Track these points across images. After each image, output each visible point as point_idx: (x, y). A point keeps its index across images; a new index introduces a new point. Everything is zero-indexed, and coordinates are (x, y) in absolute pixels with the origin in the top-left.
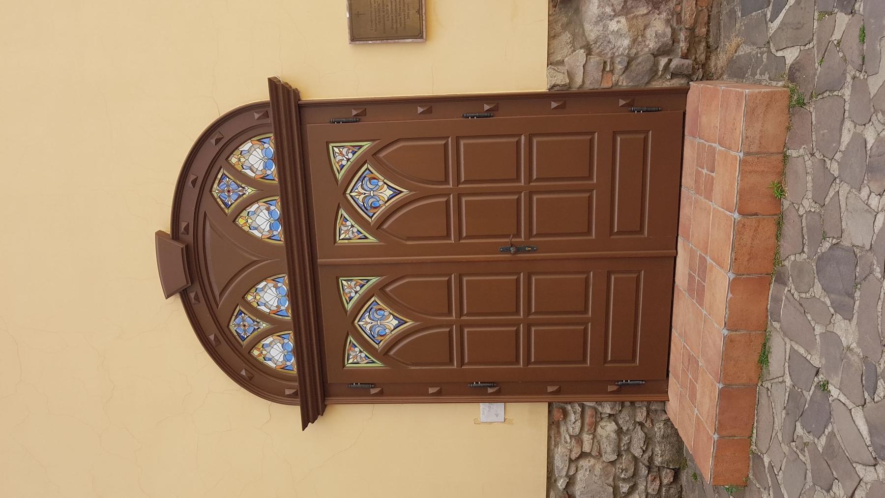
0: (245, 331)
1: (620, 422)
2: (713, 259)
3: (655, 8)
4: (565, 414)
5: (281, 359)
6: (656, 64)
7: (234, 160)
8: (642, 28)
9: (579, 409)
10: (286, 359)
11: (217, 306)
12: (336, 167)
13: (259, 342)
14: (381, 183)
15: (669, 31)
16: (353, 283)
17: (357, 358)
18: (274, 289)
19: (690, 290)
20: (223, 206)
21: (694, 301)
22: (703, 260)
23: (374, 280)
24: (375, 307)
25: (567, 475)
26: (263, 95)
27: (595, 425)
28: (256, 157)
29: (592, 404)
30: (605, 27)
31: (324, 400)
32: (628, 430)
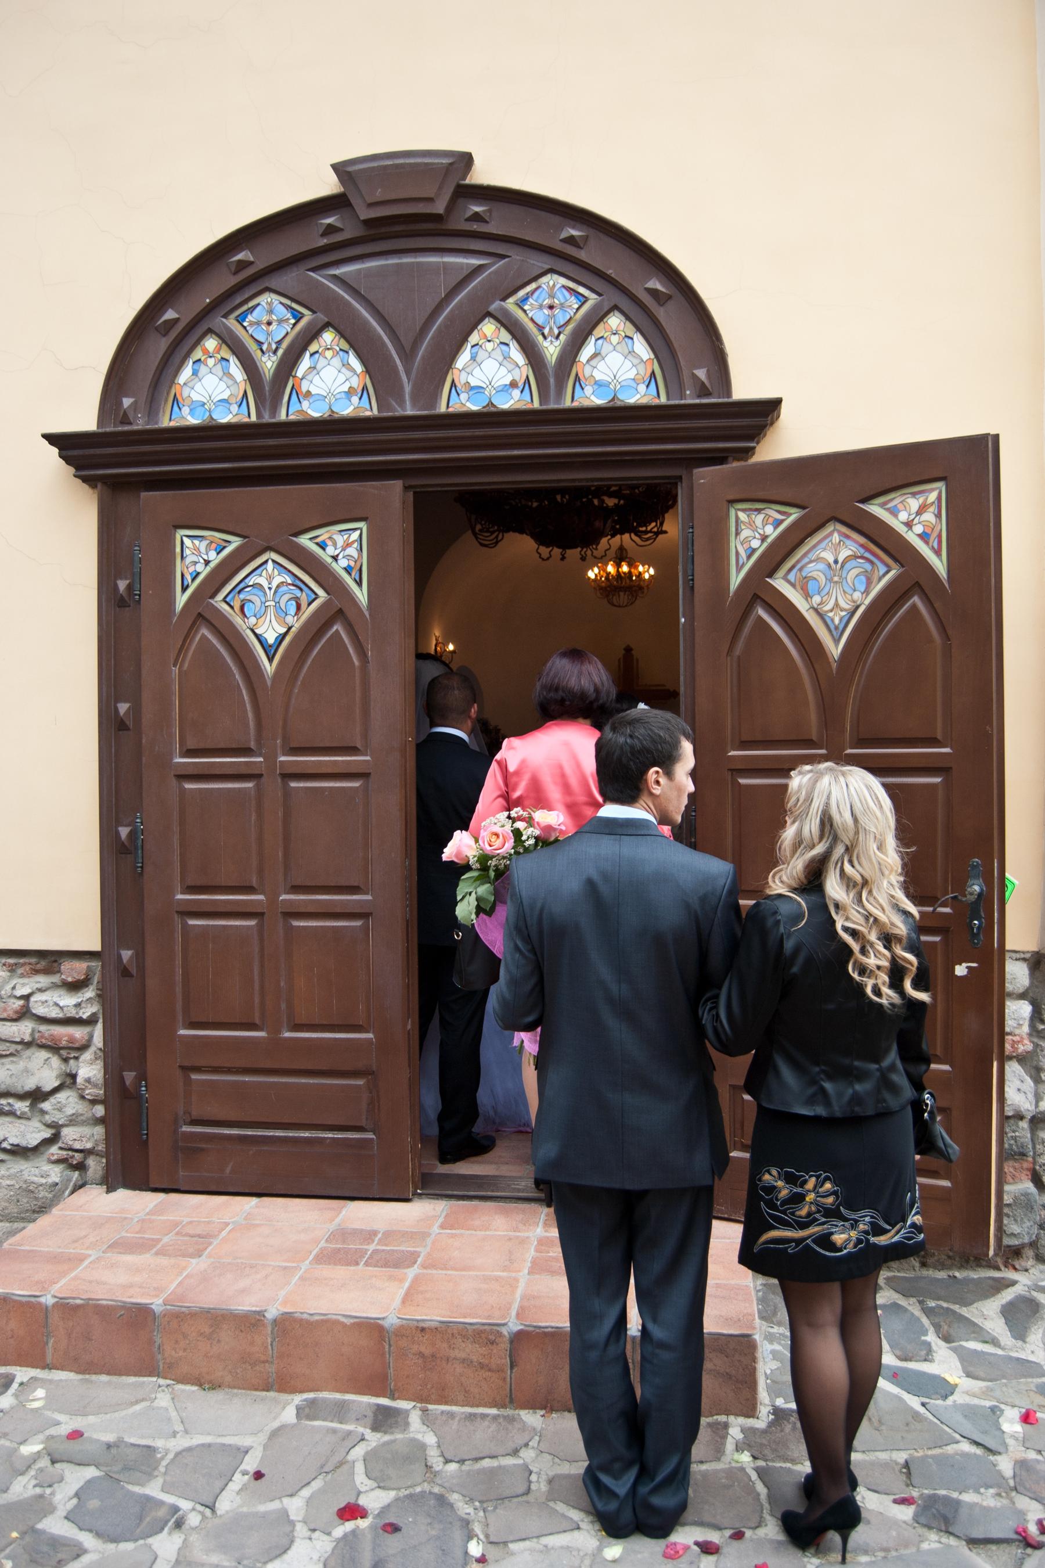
0: (258, 323)
1: (61, 1096)
2: (416, 1280)
4: (75, 987)
5: (195, 397)
7: (615, 321)
9: (86, 1013)
10: (195, 406)
11: (313, 270)
12: (323, 534)
13: (234, 353)
17: (197, 553)
19: (342, 1234)
20: (522, 293)
21: (323, 1244)
22: (410, 1259)
23: (362, 595)
27: (54, 1048)
28: (618, 369)
31: (104, 480)
32: (43, 1112)
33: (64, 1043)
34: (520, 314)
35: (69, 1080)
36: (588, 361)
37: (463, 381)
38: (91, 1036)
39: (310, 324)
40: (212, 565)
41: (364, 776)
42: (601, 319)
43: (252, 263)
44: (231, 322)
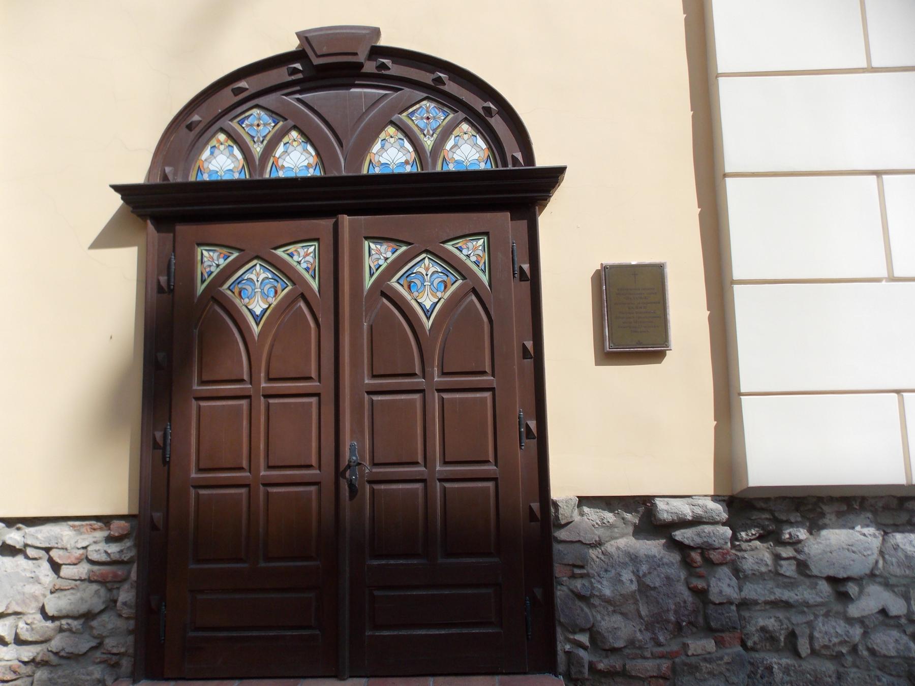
0: (251, 125)
1: (105, 617)
3: (647, 626)
6: (582, 630)
8: (624, 610)
9: (126, 557)
10: (211, 172)
12: (292, 248)
14: (439, 294)
15: (620, 644)
16: (481, 253)
18: (306, 163)
20: (411, 110)
23: (314, 285)
24: (279, 286)
25: (26, 545)
26: (542, 160)
28: (467, 152)
29: (134, 576)
30: (624, 565)
32: (92, 628)
33: (110, 579)
34: (409, 122)
35: (111, 605)
36: (452, 148)
37: (376, 160)
38: (129, 572)
39: (282, 127)
40: (221, 267)
41: (318, 395)
42: (457, 125)
43: (247, 89)
44: (234, 124)
